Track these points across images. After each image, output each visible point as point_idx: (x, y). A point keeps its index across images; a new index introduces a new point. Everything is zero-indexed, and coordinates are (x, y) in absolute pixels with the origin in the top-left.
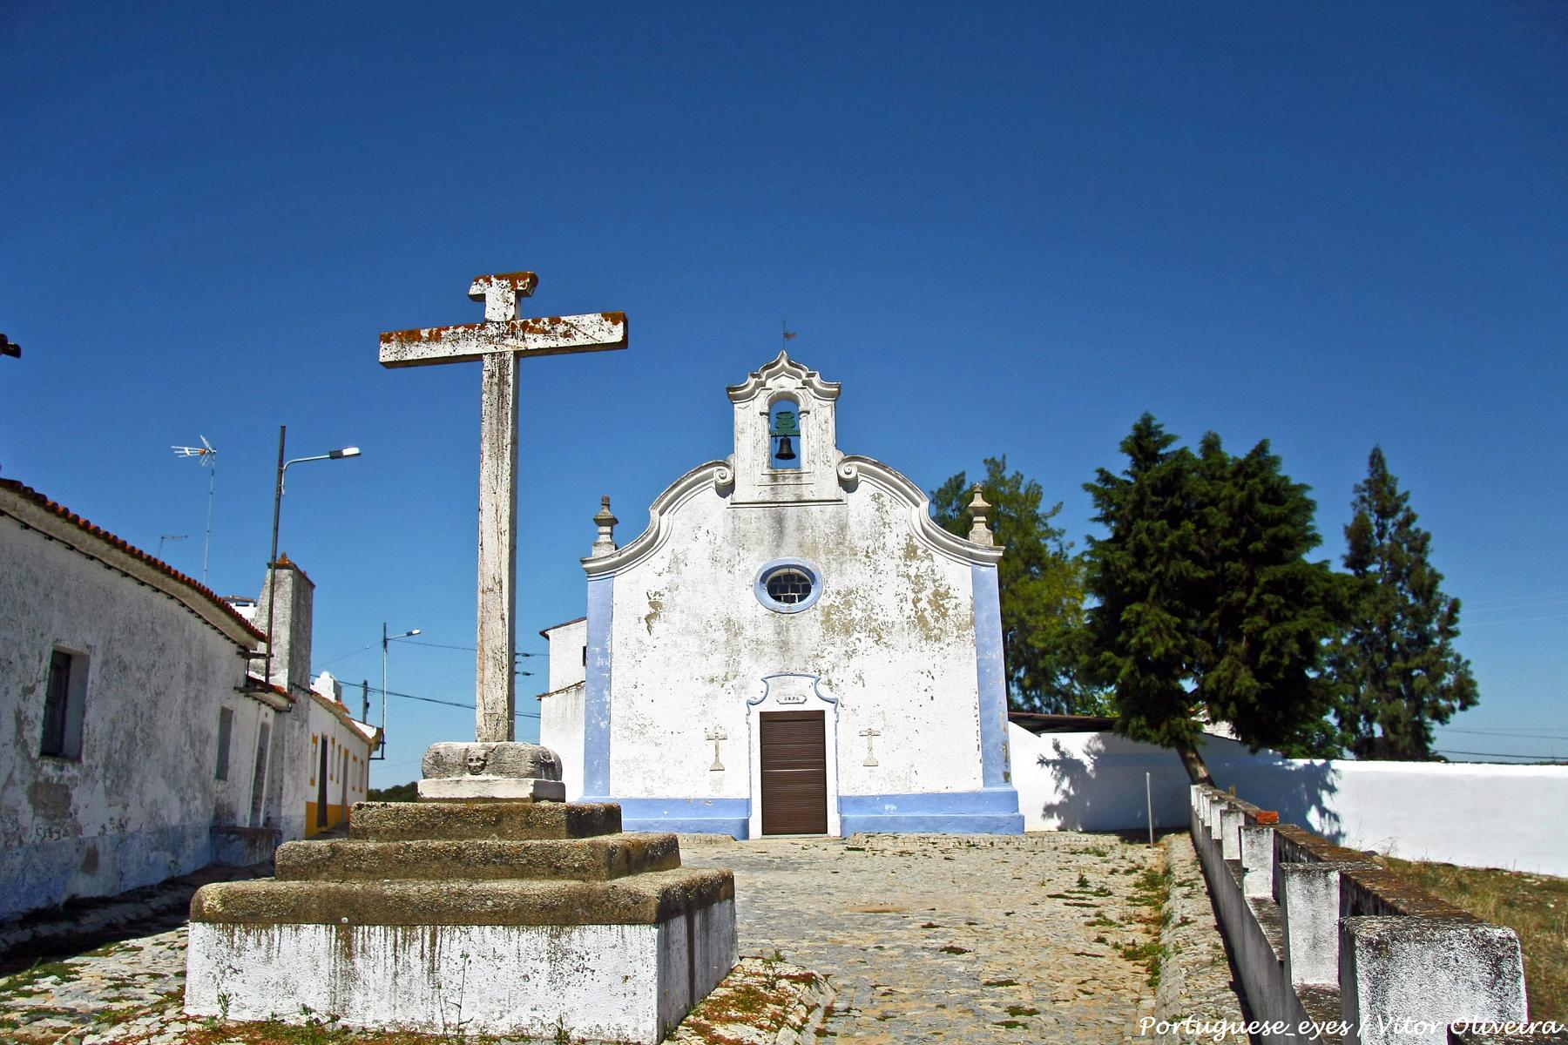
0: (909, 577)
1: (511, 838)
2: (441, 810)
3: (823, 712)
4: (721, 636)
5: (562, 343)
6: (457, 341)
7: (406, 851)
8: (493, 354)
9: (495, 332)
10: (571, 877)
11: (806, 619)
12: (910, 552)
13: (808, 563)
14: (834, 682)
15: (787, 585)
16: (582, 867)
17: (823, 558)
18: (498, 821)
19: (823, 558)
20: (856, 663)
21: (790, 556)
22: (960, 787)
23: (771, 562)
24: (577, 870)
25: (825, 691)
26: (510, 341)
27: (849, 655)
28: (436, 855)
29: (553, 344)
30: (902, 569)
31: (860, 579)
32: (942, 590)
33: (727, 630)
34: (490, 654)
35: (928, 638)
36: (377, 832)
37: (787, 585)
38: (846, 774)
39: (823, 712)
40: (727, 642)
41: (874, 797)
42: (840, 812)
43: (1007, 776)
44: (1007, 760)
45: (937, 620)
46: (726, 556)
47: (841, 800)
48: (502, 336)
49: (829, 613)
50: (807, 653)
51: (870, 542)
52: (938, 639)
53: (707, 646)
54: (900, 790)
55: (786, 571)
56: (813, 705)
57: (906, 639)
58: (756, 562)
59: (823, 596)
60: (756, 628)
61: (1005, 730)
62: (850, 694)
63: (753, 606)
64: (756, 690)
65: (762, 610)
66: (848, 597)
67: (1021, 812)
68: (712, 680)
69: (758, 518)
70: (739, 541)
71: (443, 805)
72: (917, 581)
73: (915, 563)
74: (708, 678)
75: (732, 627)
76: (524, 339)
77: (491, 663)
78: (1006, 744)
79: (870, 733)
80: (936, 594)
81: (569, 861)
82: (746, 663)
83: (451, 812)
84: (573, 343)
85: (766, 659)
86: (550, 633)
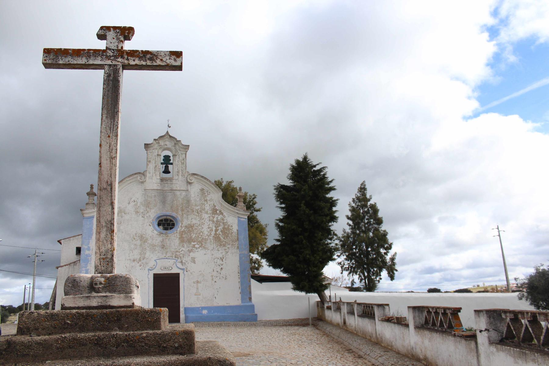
0: (213, 221)
1: (127, 329)
2: (82, 315)
3: (179, 274)
4: (139, 242)
5: (149, 63)
6: (90, 56)
7: (63, 341)
8: (110, 65)
9: (112, 54)
10: (174, 353)
11: (174, 236)
12: (214, 211)
13: (174, 214)
14: (184, 261)
15: (166, 223)
16: (180, 346)
17: (180, 213)
18: (119, 320)
19: (180, 213)
20: (192, 254)
21: (167, 212)
22: (232, 304)
23: (160, 213)
24: (177, 348)
25: (180, 265)
26: (120, 60)
27: (190, 251)
28: (81, 343)
29: (144, 63)
30: (211, 218)
31: (194, 221)
32: (226, 227)
33: (141, 240)
34: (104, 224)
35: (221, 245)
36: (37, 329)
37: (166, 223)
38: (188, 298)
39: (179, 274)
40: (141, 245)
41: (199, 308)
42: (185, 313)
43: (250, 299)
44: (250, 293)
45: (224, 238)
46: (142, 211)
47: (186, 309)
48: (116, 57)
49: (182, 234)
50: (173, 250)
51: (199, 207)
52: (224, 246)
53: (133, 246)
54: (209, 304)
55: (165, 217)
56: (174, 271)
57: (211, 245)
58: (154, 213)
59: (179, 228)
60: (153, 240)
61: (250, 281)
62: (191, 266)
63: (152, 232)
64: (152, 264)
65: (156, 232)
66: (190, 227)
67: (256, 313)
68: (134, 261)
69: (155, 196)
70: (147, 205)
71: (79, 311)
72: (217, 224)
73: (216, 216)
74: (132, 259)
75: (142, 238)
76: (128, 59)
77: (105, 229)
78: (250, 286)
79: (198, 282)
80: (224, 228)
81: (171, 343)
82: (148, 254)
83: (88, 315)
84: (155, 64)
85: (157, 252)
86: (62, 242)
